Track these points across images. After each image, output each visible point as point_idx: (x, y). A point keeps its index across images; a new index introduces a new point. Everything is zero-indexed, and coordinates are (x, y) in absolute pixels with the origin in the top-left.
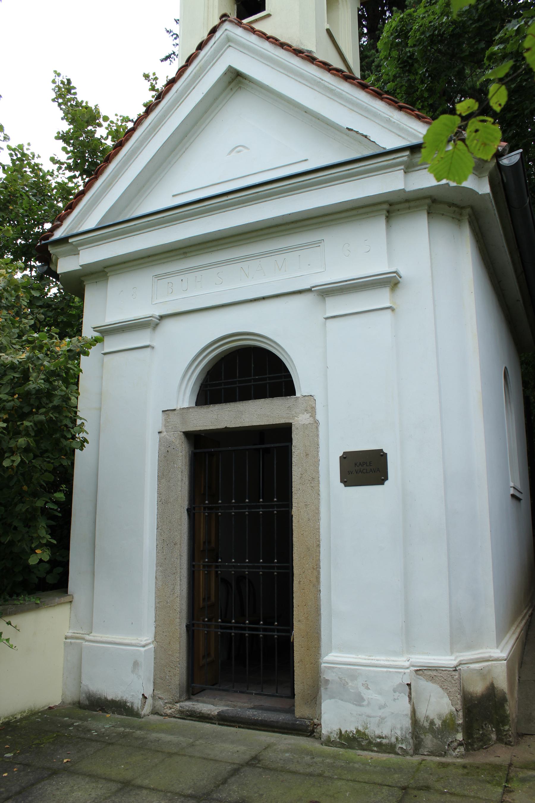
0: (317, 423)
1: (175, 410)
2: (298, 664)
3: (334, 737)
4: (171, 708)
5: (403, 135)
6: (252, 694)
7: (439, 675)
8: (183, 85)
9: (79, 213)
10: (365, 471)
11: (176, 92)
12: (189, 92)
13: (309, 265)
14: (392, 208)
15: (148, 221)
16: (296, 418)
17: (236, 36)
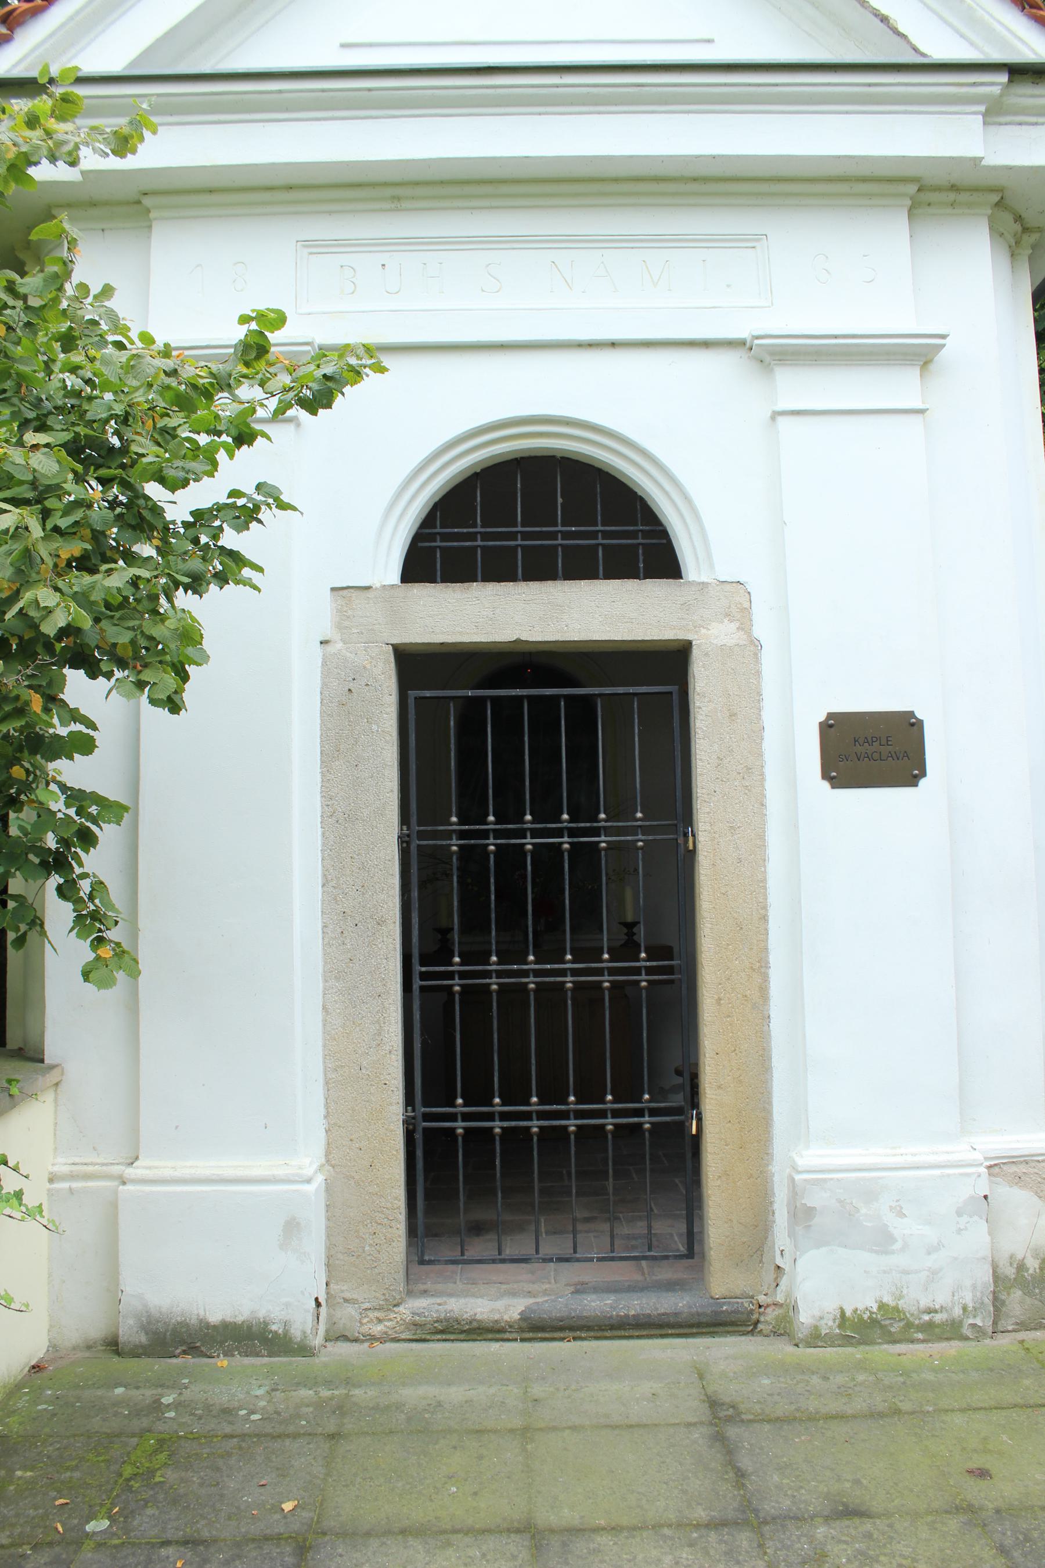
0: (755, 646)
1: (368, 588)
2: (719, 1182)
3: (829, 1325)
4: (380, 1321)
6: (591, 1260)
7: (1032, 1170)
13: (728, 286)
14: (929, 194)
15: (323, 91)
16: (703, 631)
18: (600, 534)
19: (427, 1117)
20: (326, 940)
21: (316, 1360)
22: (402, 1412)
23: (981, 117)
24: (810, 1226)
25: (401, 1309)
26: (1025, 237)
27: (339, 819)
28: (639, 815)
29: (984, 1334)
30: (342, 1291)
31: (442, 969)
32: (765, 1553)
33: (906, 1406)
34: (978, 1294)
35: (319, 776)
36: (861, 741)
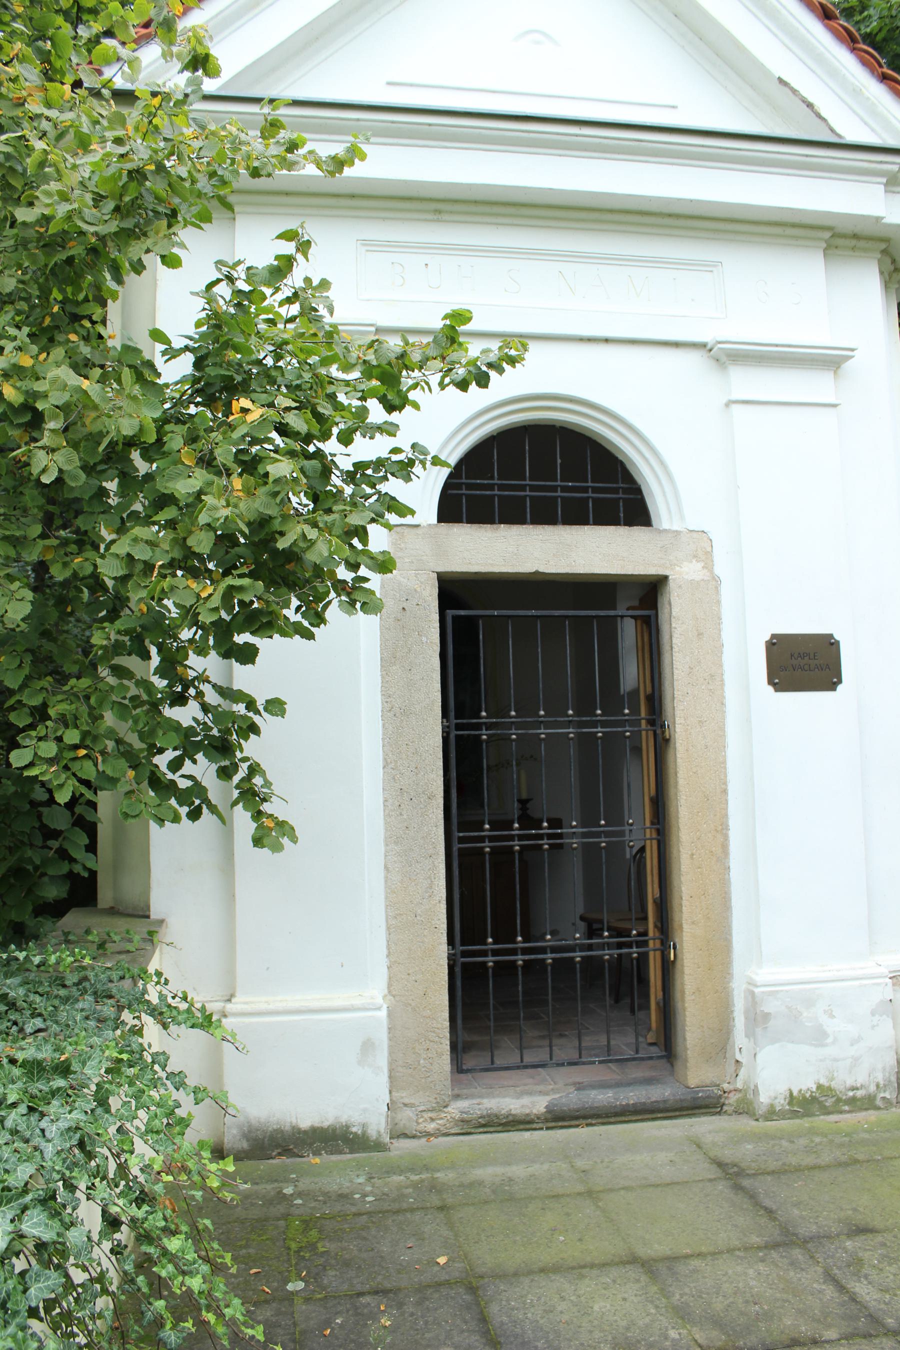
0: (716, 581)
2: (693, 997)
3: (781, 1103)
4: (432, 1120)
5: (874, 125)
6: (593, 1063)
10: (806, 667)
14: (840, 239)
15: (393, 122)
16: (678, 568)
18: (591, 490)
19: (464, 954)
20: (387, 811)
21: (391, 1154)
22: (485, 1187)
23: (882, 187)
24: (766, 1028)
25: (449, 1109)
26: (895, 275)
27: (395, 713)
28: (513, 713)
29: (891, 1104)
30: (402, 1098)
31: (476, 834)
32: (818, 1262)
33: (861, 1157)
34: (887, 1074)
35: (380, 678)
36: (796, 656)
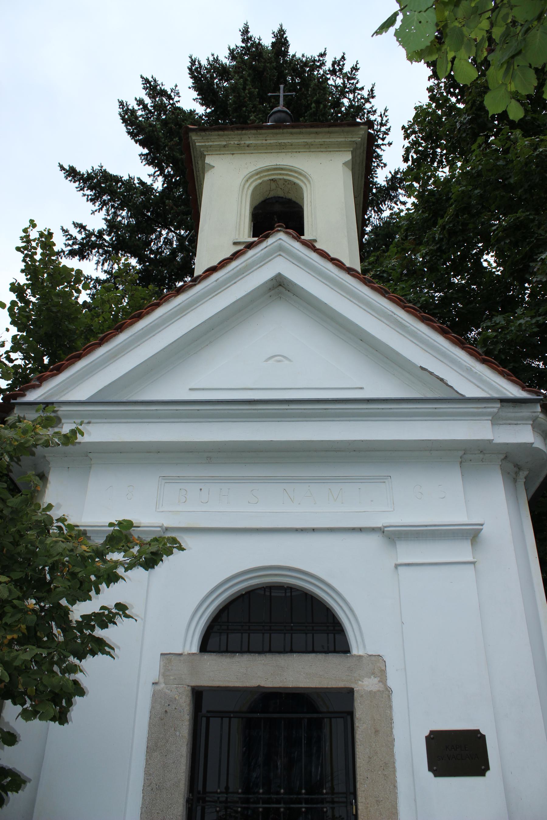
0: (388, 692)
8: (225, 276)
9: (68, 378)
11: (216, 281)
12: (229, 285)
13: (372, 501)
14: (469, 457)
16: (360, 682)
17: (292, 248)
